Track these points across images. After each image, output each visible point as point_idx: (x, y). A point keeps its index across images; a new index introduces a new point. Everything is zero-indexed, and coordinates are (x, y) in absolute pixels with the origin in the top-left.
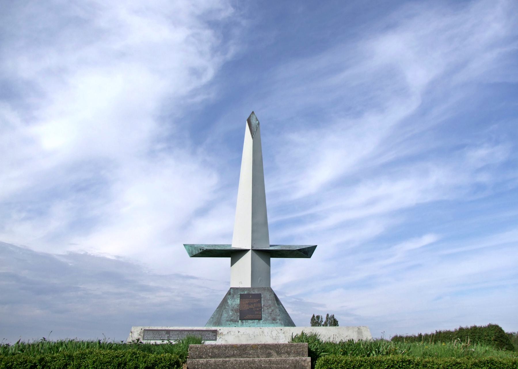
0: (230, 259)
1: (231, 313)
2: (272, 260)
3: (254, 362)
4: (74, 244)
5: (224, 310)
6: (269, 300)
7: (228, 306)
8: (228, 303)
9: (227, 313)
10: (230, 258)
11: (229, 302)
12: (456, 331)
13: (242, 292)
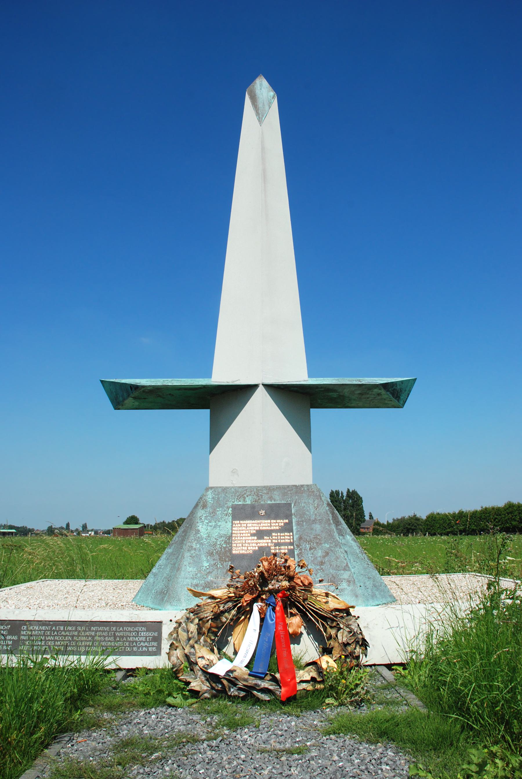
0: (206, 413)
1: (206, 564)
5: (187, 554)
6: (314, 522)
7: (199, 540)
9: (196, 560)
10: (208, 411)
12: (475, 513)
13: (238, 499)
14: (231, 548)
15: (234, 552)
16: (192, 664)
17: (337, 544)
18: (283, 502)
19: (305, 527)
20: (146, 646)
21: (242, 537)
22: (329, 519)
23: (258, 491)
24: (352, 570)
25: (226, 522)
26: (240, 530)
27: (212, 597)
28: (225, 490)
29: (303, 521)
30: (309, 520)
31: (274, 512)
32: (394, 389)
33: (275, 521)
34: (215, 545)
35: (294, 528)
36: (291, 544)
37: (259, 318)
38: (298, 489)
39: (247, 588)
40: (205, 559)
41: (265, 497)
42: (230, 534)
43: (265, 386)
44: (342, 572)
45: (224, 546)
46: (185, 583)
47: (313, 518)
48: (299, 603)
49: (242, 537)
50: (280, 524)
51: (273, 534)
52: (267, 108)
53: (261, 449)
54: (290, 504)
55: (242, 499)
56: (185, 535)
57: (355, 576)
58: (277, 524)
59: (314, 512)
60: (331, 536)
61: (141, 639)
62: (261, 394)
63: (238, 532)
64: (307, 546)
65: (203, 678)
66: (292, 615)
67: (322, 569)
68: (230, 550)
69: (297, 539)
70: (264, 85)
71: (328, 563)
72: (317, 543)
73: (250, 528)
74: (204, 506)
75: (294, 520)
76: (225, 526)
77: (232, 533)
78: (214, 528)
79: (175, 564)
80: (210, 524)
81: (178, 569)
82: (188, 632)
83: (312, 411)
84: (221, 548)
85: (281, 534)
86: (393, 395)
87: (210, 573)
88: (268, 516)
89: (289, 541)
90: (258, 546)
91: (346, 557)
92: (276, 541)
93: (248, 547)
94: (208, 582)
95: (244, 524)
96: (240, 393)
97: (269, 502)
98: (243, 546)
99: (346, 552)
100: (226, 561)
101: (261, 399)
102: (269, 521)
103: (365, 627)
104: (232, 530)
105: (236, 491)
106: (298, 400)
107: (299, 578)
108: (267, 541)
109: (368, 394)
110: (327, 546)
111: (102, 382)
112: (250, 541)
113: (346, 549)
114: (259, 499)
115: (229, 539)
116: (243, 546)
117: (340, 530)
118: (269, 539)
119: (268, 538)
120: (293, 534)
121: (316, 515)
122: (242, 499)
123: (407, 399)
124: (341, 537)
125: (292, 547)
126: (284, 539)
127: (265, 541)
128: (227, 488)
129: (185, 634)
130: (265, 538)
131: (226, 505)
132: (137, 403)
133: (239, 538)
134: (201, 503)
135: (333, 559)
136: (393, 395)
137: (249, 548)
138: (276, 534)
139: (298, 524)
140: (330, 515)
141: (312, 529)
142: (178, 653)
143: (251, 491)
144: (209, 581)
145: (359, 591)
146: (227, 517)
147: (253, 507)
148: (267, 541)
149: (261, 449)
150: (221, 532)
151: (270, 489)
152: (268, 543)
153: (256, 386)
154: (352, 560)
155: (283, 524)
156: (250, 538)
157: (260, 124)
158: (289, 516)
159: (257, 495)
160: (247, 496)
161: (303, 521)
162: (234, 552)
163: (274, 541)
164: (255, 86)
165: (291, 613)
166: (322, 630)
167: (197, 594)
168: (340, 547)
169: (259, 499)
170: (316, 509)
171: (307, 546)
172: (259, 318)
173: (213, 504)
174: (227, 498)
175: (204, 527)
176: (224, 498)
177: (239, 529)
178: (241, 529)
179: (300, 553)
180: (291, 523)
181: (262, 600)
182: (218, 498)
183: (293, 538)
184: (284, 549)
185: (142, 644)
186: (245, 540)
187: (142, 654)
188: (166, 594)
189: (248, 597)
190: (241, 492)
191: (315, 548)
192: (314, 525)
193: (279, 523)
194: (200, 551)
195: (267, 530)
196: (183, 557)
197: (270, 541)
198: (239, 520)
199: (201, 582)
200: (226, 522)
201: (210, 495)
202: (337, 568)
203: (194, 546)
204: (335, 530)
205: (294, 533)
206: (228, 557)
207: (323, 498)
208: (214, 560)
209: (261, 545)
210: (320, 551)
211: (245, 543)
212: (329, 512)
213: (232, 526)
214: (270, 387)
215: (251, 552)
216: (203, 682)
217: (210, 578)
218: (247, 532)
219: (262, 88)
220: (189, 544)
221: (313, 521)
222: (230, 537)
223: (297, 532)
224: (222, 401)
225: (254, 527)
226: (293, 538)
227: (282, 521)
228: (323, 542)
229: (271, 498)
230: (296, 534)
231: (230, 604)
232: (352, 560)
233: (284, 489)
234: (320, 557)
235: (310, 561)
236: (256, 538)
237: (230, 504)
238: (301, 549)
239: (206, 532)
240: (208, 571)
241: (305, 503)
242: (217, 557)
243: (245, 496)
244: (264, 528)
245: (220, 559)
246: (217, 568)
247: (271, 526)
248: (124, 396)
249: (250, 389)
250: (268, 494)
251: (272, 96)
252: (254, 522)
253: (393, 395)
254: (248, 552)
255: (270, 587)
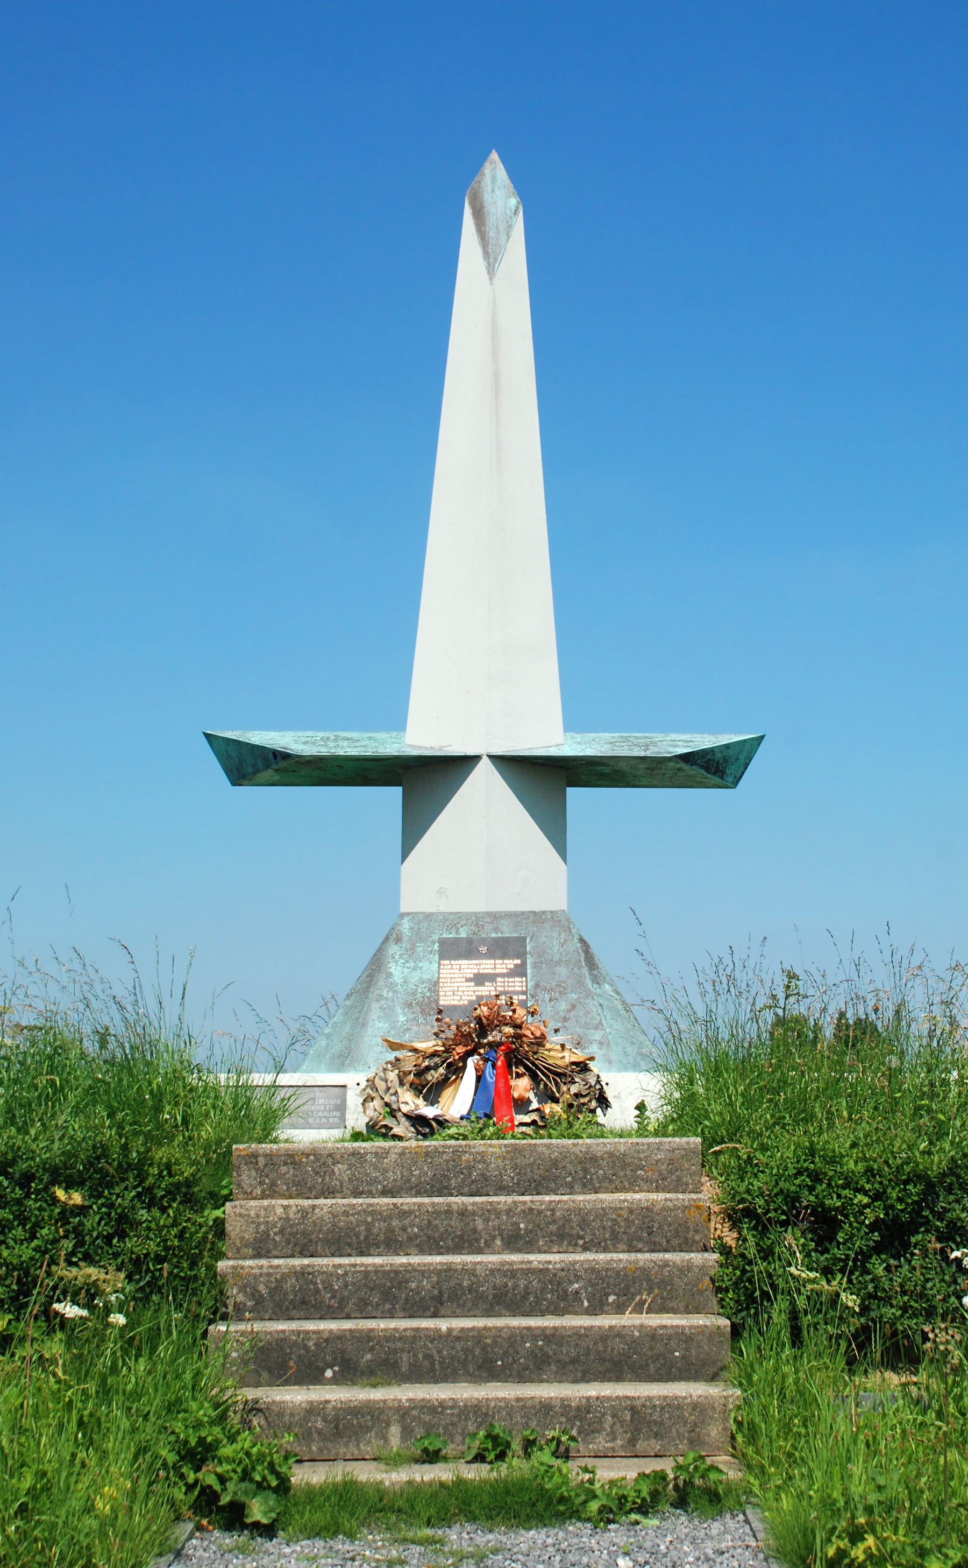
1: (402, 1018)
2: (573, 793)
3: (637, 1261)
4: (494, 298)
5: (375, 1006)
6: (558, 963)
7: (392, 986)
8: (390, 975)
9: (388, 1013)
11: (397, 971)
13: (449, 930)
15: (441, 1003)
16: (393, 1113)
17: (589, 995)
18: (514, 935)
20: (325, 1117)
22: (580, 960)
23: (477, 919)
24: (608, 1030)
27: (415, 1050)
28: (428, 916)
29: (542, 963)
31: (500, 948)
32: (709, 760)
33: (501, 961)
34: (414, 993)
35: (529, 971)
36: (524, 993)
37: (484, 662)
38: (538, 917)
39: (462, 1037)
40: (400, 1011)
41: (488, 927)
42: (435, 979)
43: (491, 757)
44: (593, 1031)
46: (374, 1043)
47: (556, 958)
48: (528, 1060)
50: (509, 966)
51: (499, 979)
52: (503, 237)
53: (484, 852)
54: (524, 939)
55: (453, 931)
56: (372, 980)
57: (610, 1037)
58: (504, 966)
60: (581, 983)
61: (318, 1108)
62: (484, 772)
63: (448, 976)
65: (407, 1123)
66: (519, 1076)
68: (437, 1001)
70: (499, 180)
71: (574, 1020)
72: (560, 992)
73: (466, 971)
74: (398, 940)
75: (529, 961)
76: (429, 967)
77: (439, 978)
79: (357, 1019)
80: (407, 965)
81: (364, 1025)
82: (386, 1081)
83: (570, 790)
84: (423, 997)
86: (714, 768)
88: (491, 955)
91: (600, 1012)
96: (452, 768)
97: (494, 935)
99: (601, 1005)
101: (485, 777)
102: (493, 961)
103: (615, 1097)
105: (446, 920)
106: (544, 779)
107: (528, 1029)
108: (490, 988)
109: (661, 768)
110: (574, 996)
111: (207, 736)
112: (464, 989)
113: (601, 1002)
115: (435, 985)
117: (596, 976)
121: (561, 954)
122: (453, 931)
123: (743, 773)
124: (595, 986)
125: (524, 997)
127: (485, 988)
128: (432, 914)
129: (383, 1083)
130: (487, 984)
132: (277, 777)
133: (449, 984)
134: (394, 936)
135: (581, 1013)
136: (714, 768)
139: (535, 966)
140: (583, 955)
141: (555, 973)
142: (377, 1103)
143: (468, 919)
145: (614, 1057)
147: (469, 941)
148: (490, 988)
149: (484, 852)
150: (424, 976)
151: (495, 917)
153: (477, 758)
154: (608, 1017)
155: (512, 966)
156: (466, 984)
157: (491, 279)
158: (522, 955)
159: (477, 925)
162: (441, 1003)
163: (498, 988)
164: (483, 184)
165: (517, 1073)
166: (555, 1090)
167: (394, 1046)
168: (593, 999)
172: (484, 662)
175: (398, 968)
177: (449, 971)
178: (452, 971)
180: (524, 964)
181: (480, 1054)
182: (419, 929)
183: (526, 986)
185: (320, 1114)
187: (320, 1127)
188: (347, 1057)
189: (460, 1049)
190: (452, 920)
194: (393, 1000)
196: (369, 1008)
197: (493, 988)
198: (450, 959)
201: (406, 925)
202: (587, 1026)
203: (385, 995)
204: (587, 975)
205: (529, 978)
207: (573, 931)
209: (480, 993)
212: (580, 951)
214: (501, 761)
215: (466, 1002)
216: (407, 1129)
219: (496, 184)
220: (378, 992)
222: (437, 983)
224: (425, 780)
226: (526, 986)
229: (496, 930)
231: (437, 1059)
232: (608, 1017)
233: (517, 917)
236: (473, 984)
237: (436, 937)
242: (418, 1009)
243: (459, 926)
244: (486, 971)
246: (418, 1025)
247: (495, 968)
248: (249, 765)
249: (465, 763)
251: (513, 209)
252: (470, 962)
253: (707, 769)
254: (461, 1003)
255: (490, 1038)
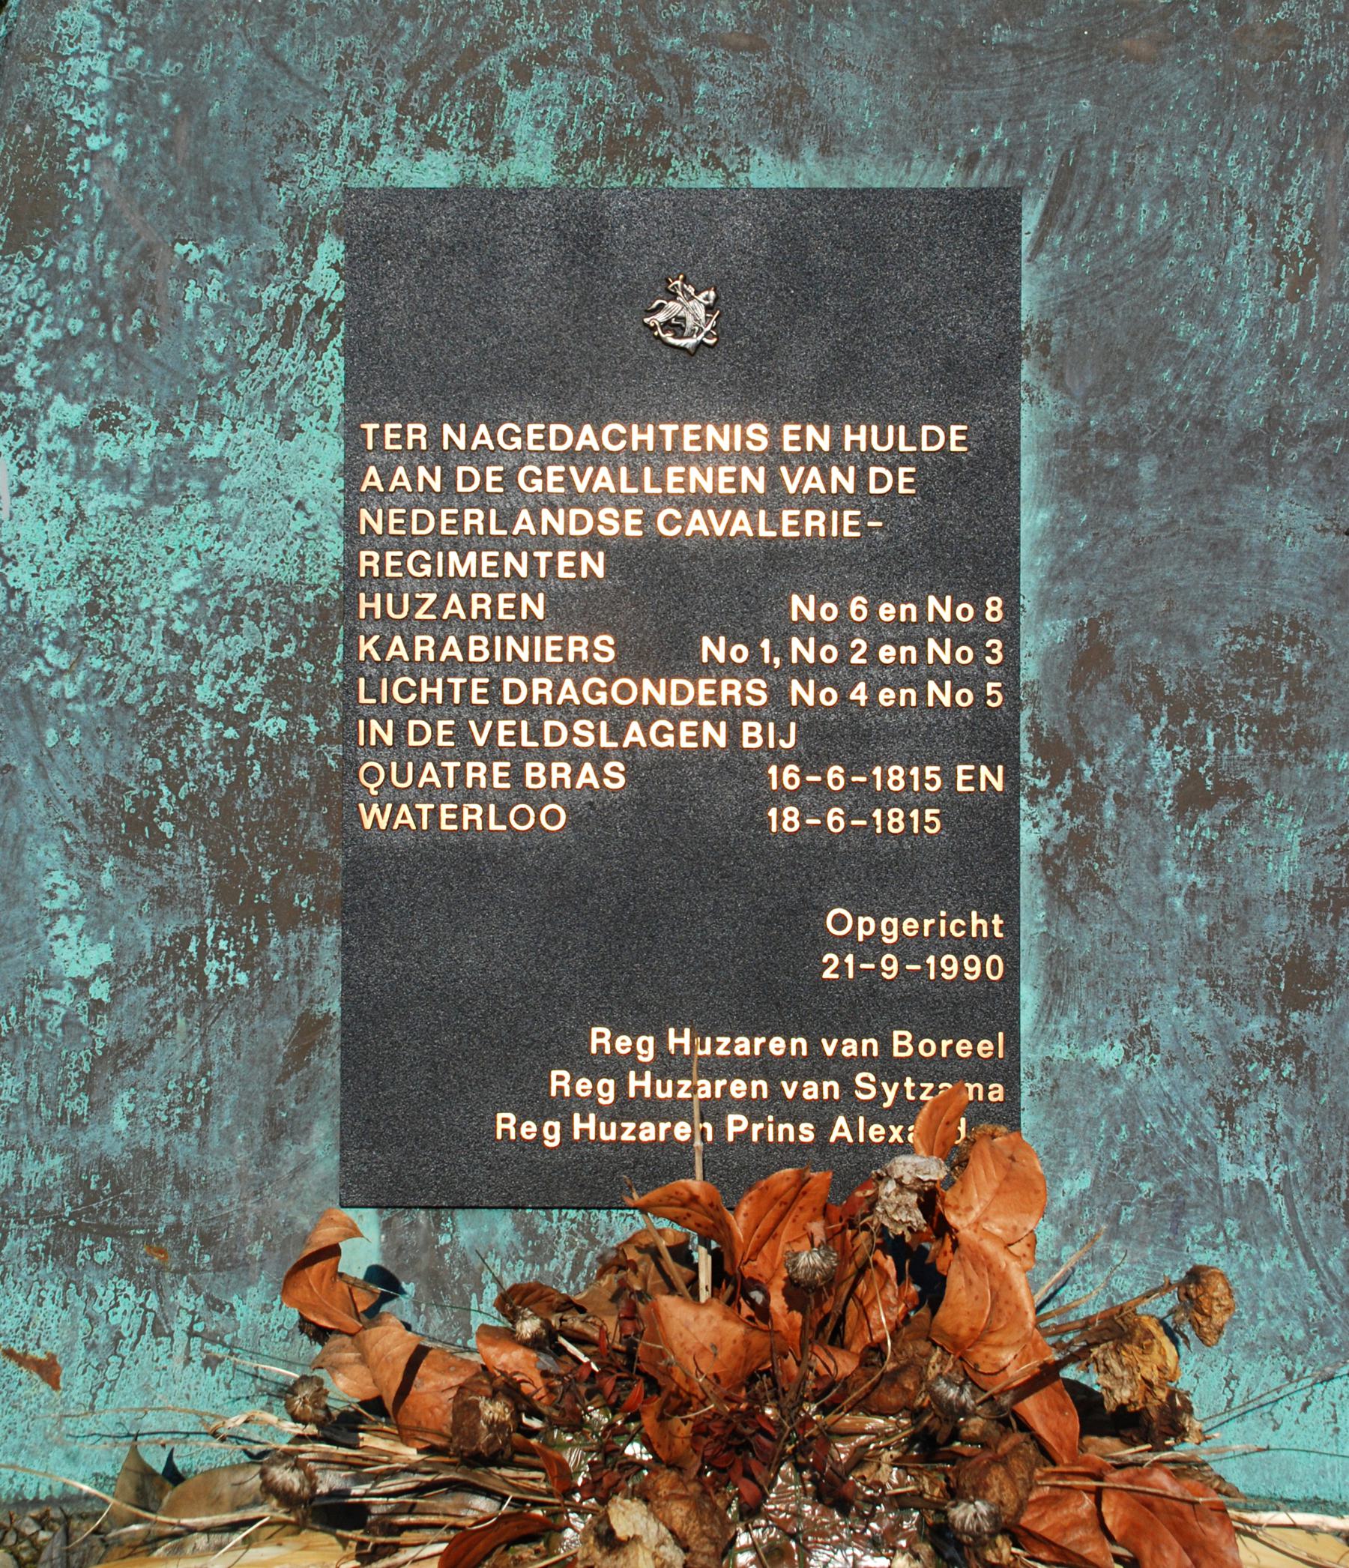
1: (79, 954)
6: (1260, 452)
14: (349, 764)
19: (1151, 516)
21: (465, 628)
25: (288, 430)
26: (438, 543)
30: (1208, 425)
34: (171, 713)
36: (989, 736)
45: (272, 726)
47: (1246, 402)
49: (465, 628)
50: (881, 482)
54: (995, 212)
55: (455, 118)
59: (1263, 326)
64: (1160, 758)
67: (1295, 1048)
68: (339, 790)
69: (1047, 660)
78: (154, 496)
80: (108, 448)
84: (234, 755)
85: (886, 612)
87: (122, 1056)
88: (741, 374)
89: (965, 699)
90: (631, 756)
92: (829, 697)
93: (518, 757)
94: (106, 1168)
95: (481, 457)
97: (768, 172)
98: (465, 748)
100: (290, 918)
102: (758, 434)
104: (354, 537)
108: (730, 690)
114: (653, 121)
116: (465, 748)
118: (755, 666)
119: (740, 653)
120: (1012, 609)
121: (1284, 364)
122: (455, 118)
126: (914, 676)
130: (595, 565)
131: (280, 198)
137: (534, 773)
138: (829, 611)
139: (1074, 478)
141: (1225, 549)
144: (114, 1150)
146: (291, 361)
147: (580, 230)
148: (730, 690)
150: (238, 558)
152: (733, 716)
158: (977, 377)
159: (635, 65)
160: (522, 76)
161: (1128, 442)
162: (372, 817)
169: (653, 121)
170: (1301, 283)
171: (1160, 758)
173: (129, 172)
174: (288, 94)
176: (256, 90)
179: (1080, 843)
182: (190, 96)
183: (1011, 665)
184: (906, 800)
186: (496, 670)
191: (1242, 790)
192: (1251, 492)
193: (864, 460)
195: (724, 554)
197: (757, 691)
199: (31, 1170)
200: (288, 430)
206: (311, 863)
208: (163, 898)
210: (1291, 831)
211: (496, 707)
213: (351, 471)
217: (118, 1126)
218: (516, 564)
221: (1250, 440)
223: (1057, 575)
225: (593, 501)
227: (898, 436)
228: (1329, 720)
230: (1048, 605)
234: (1288, 899)
235: (1173, 946)
237: (323, 179)
238: (1084, 800)
239: (70, 553)
240: (104, 1031)
241: (1174, 190)
242: (191, 864)
243: (498, 64)
245: (224, 893)
250: (758, 45)
